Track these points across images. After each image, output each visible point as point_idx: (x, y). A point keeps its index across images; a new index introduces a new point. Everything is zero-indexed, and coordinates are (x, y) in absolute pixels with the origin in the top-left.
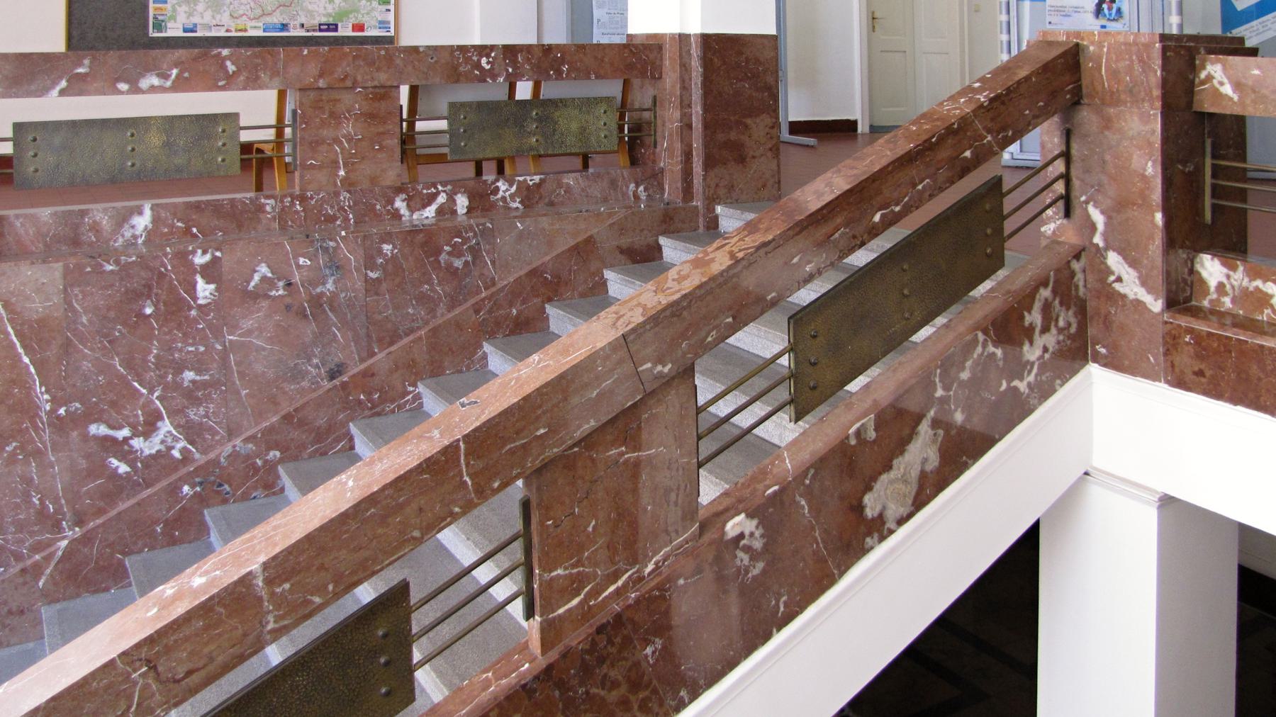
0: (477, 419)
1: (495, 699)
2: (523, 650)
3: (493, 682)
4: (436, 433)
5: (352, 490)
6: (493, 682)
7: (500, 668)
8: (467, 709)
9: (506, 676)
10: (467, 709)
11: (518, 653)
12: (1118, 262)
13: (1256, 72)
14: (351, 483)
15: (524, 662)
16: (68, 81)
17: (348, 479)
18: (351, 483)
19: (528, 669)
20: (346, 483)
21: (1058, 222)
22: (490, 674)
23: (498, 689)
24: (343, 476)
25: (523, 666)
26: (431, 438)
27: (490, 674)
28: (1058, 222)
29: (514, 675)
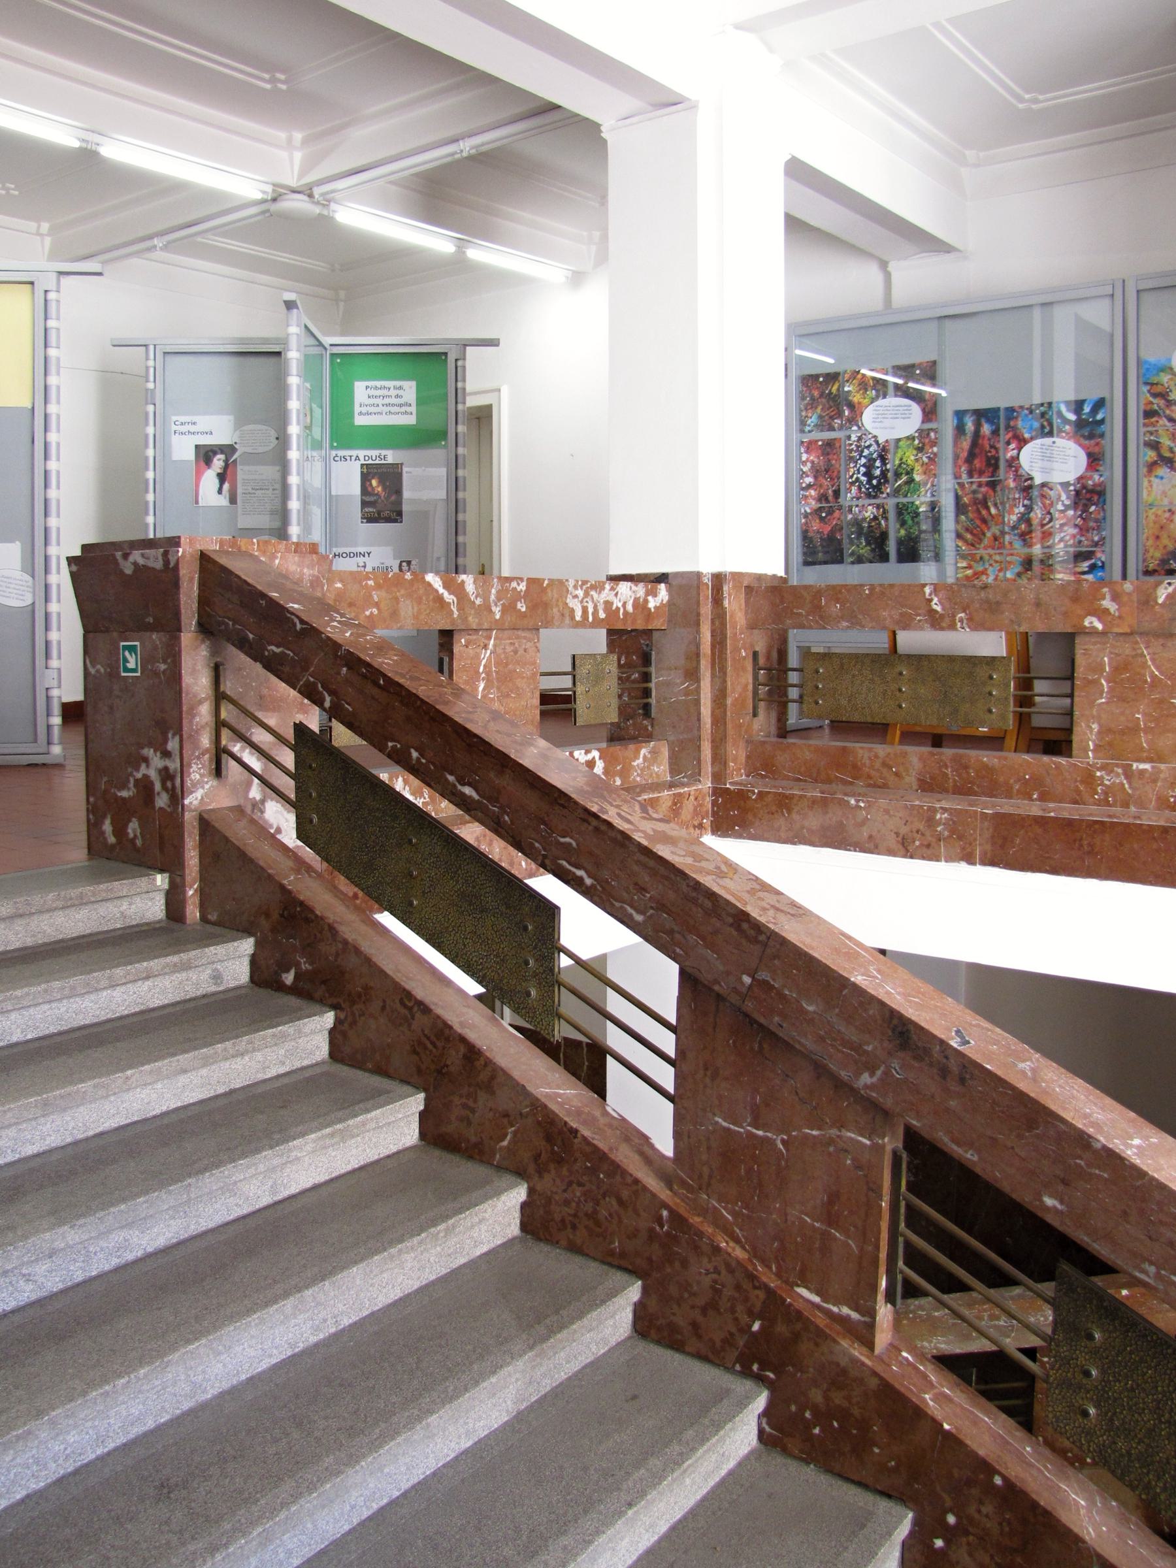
0: (989, 1030)
1: (958, 1385)
2: (884, 1363)
3: (936, 1391)
4: (1025, 1066)
5: (1147, 1138)
6: (936, 1391)
7: (914, 1385)
8: (981, 1415)
9: (925, 1376)
10: (981, 1415)
11: (889, 1365)
12: (277, 812)
13: (339, 585)
14: (1136, 1142)
15: (900, 1358)
16: (143, 748)
17: (1132, 1146)
18: (1136, 1142)
19: (909, 1352)
20: (1138, 1147)
21: (207, 786)
22: (927, 1396)
23: (944, 1383)
24: (1129, 1152)
25: (907, 1359)
26: (1033, 1070)
27: (927, 1396)
28: (207, 786)
29: (921, 1368)
